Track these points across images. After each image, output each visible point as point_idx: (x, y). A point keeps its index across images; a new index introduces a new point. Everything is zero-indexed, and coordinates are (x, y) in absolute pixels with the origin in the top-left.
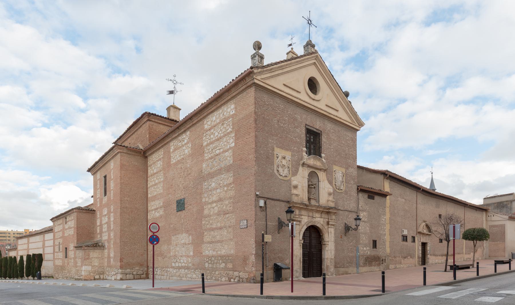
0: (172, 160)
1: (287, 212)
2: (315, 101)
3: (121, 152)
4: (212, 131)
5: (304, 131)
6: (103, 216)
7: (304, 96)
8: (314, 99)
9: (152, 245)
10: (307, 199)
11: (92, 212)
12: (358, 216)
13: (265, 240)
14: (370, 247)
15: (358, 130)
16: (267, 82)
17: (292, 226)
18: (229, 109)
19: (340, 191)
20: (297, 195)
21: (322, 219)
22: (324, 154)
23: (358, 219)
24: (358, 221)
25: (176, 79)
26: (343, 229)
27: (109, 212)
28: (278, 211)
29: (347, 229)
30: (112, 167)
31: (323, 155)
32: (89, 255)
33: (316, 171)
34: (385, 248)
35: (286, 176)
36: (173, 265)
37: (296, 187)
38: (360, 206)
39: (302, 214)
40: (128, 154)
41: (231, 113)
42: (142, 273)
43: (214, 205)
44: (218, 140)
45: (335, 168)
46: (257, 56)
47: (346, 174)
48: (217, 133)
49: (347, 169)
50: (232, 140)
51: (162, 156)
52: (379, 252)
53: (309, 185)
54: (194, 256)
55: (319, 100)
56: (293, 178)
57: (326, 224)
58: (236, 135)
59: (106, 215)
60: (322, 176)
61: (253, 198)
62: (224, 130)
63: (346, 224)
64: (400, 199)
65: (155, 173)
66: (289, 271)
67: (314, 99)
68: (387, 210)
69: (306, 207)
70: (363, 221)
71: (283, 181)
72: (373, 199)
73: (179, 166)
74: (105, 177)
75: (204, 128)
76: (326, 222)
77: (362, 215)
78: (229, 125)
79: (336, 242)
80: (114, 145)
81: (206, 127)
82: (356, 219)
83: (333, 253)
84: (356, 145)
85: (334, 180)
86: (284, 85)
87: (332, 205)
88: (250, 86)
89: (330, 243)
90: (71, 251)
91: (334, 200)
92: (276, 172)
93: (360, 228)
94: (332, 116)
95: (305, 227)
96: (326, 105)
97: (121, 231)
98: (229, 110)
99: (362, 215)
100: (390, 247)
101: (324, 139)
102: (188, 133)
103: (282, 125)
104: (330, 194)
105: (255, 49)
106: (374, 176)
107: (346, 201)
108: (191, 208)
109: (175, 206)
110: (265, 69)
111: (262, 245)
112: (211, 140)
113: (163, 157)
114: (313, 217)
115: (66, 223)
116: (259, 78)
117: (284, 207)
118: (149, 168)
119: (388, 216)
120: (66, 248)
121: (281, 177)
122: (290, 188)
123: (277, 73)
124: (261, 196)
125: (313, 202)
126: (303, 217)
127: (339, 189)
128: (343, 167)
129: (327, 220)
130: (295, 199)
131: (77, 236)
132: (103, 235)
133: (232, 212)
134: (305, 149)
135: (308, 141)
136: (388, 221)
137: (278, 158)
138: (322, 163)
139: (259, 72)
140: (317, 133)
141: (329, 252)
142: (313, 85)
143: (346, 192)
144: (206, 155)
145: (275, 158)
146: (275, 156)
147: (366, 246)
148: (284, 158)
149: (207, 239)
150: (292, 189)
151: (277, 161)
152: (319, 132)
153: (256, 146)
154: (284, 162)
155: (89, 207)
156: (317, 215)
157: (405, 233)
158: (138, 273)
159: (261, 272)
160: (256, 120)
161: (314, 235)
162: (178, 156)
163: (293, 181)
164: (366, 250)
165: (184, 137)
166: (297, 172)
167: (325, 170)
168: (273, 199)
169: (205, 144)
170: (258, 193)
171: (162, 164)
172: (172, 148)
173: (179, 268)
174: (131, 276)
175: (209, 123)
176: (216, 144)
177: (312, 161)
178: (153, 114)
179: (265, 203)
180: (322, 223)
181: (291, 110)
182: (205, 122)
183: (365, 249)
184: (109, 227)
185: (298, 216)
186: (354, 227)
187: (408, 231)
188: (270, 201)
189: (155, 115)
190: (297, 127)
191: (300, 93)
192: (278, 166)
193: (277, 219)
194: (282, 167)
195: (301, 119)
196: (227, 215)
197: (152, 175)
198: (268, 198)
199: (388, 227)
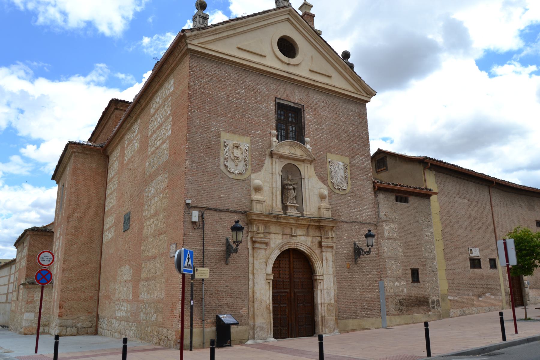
2: (290, 66)
3: (75, 152)
5: (272, 107)
7: (273, 61)
8: (288, 64)
10: (280, 205)
11: (49, 234)
14: (407, 281)
15: (368, 102)
16: (208, 46)
18: (170, 86)
20: (260, 202)
21: (310, 239)
24: (370, 239)
26: (351, 253)
28: (220, 229)
29: (358, 252)
31: (307, 139)
32: (33, 297)
33: (296, 163)
35: (241, 174)
37: (258, 189)
38: (381, 214)
39: (271, 231)
40: (84, 153)
42: (90, 325)
45: (330, 157)
46: (198, 17)
47: (352, 166)
52: (425, 288)
55: (297, 65)
56: (253, 176)
57: (317, 246)
60: (308, 172)
61: (182, 208)
62: (164, 113)
63: (355, 244)
64: (458, 199)
67: (288, 64)
68: (436, 218)
69: (272, 220)
72: (407, 202)
76: (317, 243)
77: (387, 228)
79: (338, 275)
83: (332, 294)
84: (366, 122)
87: (326, 214)
88: (185, 55)
89: (325, 278)
91: (330, 207)
92: (222, 167)
95: (277, 253)
96: (310, 70)
97: (64, 261)
101: (308, 117)
102: (139, 121)
104: (322, 197)
106: (409, 167)
108: (134, 226)
110: (204, 31)
111: (190, 288)
114: (291, 236)
116: (195, 42)
119: (437, 227)
123: (225, 34)
124: (195, 205)
125: (291, 212)
126: (272, 236)
127: (339, 189)
128: (345, 155)
129: (319, 239)
130: (257, 208)
131: (27, 268)
134: (275, 132)
135: (279, 122)
137: (226, 147)
138: (306, 150)
139: (195, 35)
140: (295, 108)
141: (326, 292)
142: (287, 47)
143: (353, 194)
145: (222, 147)
146: (222, 144)
147: (398, 279)
148: (237, 147)
150: (253, 192)
151: (225, 152)
152: (300, 107)
153: (189, 132)
154: (237, 153)
155: (48, 228)
156: (300, 232)
157: (476, 253)
158: (84, 326)
160: (189, 97)
163: (254, 180)
164: (398, 286)
166: (262, 166)
167: (311, 162)
168: (216, 210)
170: (189, 201)
174: (74, 330)
177: (287, 149)
179: (202, 216)
180: (309, 244)
181: (249, 80)
183: (397, 284)
186: (366, 249)
190: (261, 102)
191: (265, 57)
192: (226, 159)
193: (224, 241)
194: (233, 161)
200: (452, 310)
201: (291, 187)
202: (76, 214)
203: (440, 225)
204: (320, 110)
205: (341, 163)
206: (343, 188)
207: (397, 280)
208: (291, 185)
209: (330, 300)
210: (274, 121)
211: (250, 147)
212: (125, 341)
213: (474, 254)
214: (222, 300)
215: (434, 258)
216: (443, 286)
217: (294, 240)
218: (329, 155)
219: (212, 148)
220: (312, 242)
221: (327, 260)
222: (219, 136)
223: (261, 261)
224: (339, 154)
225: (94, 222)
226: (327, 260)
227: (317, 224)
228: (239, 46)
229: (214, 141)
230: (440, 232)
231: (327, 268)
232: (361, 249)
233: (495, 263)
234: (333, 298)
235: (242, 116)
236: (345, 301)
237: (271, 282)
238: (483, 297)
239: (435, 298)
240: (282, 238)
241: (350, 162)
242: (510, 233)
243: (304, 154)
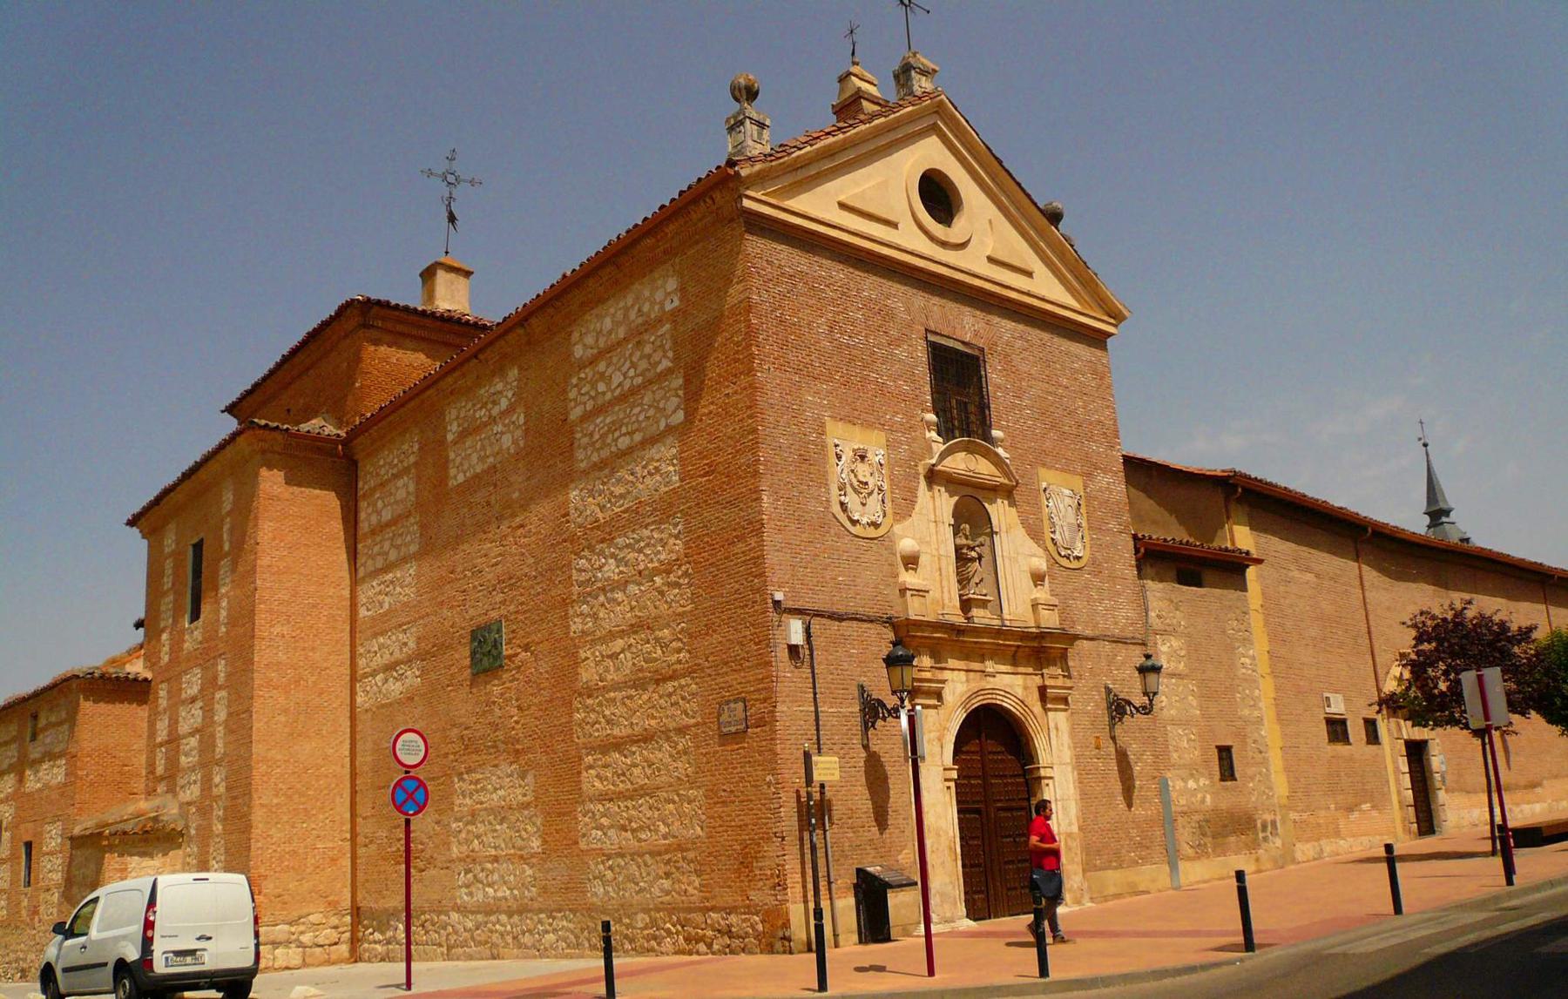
0: (453, 472)
1: (891, 661)
4: (602, 366)
5: (922, 354)
6: (183, 702)
7: (911, 237)
9: (403, 818)
12: (1148, 657)
13: (818, 777)
14: (1211, 776)
16: (791, 204)
17: (911, 720)
19: (1075, 564)
20: (921, 592)
21: (1019, 680)
22: (1000, 428)
23: (1148, 670)
24: (1152, 677)
25: (455, 166)
27: (210, 684)
29: (1118, 708)
30: (227, 507)
31: (996, 433)
34: (1268, 776)
36: (463, 896)
37: (911, 562)
38: (1152, 614)
41: (668, 307)
43: (619, 644)
44: (623, 398)
47: (1089, 498)
48: (619, 377)
49: (1088, 476)
50: (675, 400)
51: (412, 459)
53: (958, 549)
54: (545, 854)
56: (897, 528)
57: (1036, 695)
58: (687, 381)
59: (193, 700)
60: (1000, 512)
62: (643, 365)
63: (1108, 691)
64: (1296, 574)
65: (388, 525)
66: (914, 895)
68: (1256, 621)
70: (1172, 675)
71: (862, 542)
73: (479, 497)
74: (198, 548)
75: (570, 354)
77: (1164, 649)
78: (662, 346)
80: (232, 424)
81: (578, 351)
82: (1142, 670)
85: (1046, 523)
87: (1050, 620)
90: (51, 853)
93: (1162, 700)
94: (1014, 295)
95: (960, 716)
98: (659, 295)
99: (1166, 651)
100: (1287, 769)
101: (994, 375)
103: (845, 339)
104: (1038, 578)
105: (737, 100)
107: (1101, 601)
109: (463, 654)
112: (600, 402)
113: (416, 463)
115: (34, 738)
117: (881, 641)
118: (363, 504)
120: (29, 845)
121: (856, 530)
124: (790, 604)
128: (1074, 472)
130: (915, 609)
132: (181, 782)
133: (689, 672)
134: (932, 417)
136: (1264, 666)
137: (839, 457)
138: (997, 461)
140: (967, 355)
142: (937, 196)
143: (1096, 567)
144: (580, 454)
146: (832, 451)
147: (1192, 771)
149: (592, 782)
151: (839, 471)
152: (976, 353)
154: (863, 471)
157: (1338, 707)
158: (321, 941)
161: (994, 740)
162: (474, 457)
165: (500, 386)
166: (913, 503)
169: (576, 413)
171: (412, 488)
172: (454, 427)
173: (489, 910)
175: (589, 340)
176: (618, 412)
177: (960, 463)
178: (379, 302)
181: (870, 286)
182: (576, 335)
183: (1191, 784)
184: (207, 745)
185: (928, 675)
187: (1347, 700)
188: (824, 621)
189: (387, 305)
190: (895, 343)
195: (908, 311)
196: (670, 686)
197: (373, 532)
198: (819, 614)
199: (1266, 690)
200: (1299, 845)
201: (974, 554)
202: (277, 630)
203: (1265, 639)
204: (1016, 359)
205: (1067, 492)
207: (1192, 775)
208: (973, 549)
210: (928, 388)
213: (1333, 710)
215: (1260, 721)
216: (1281, 786)
217: (991, 683)
218: (1042, 472)
220: (1026, 688)
224: (1062, 470)
225: (326, 649)
227: (1035, 644)
230: (1266, 656)
232: (879, 701)
233: (1376, 731)
234: (1074, 820)
235: (864, 379)
237: (952, 784)
238: (1356, 814)
239: (1268, 817)
242: (1403, 656)
243: (997, 473)
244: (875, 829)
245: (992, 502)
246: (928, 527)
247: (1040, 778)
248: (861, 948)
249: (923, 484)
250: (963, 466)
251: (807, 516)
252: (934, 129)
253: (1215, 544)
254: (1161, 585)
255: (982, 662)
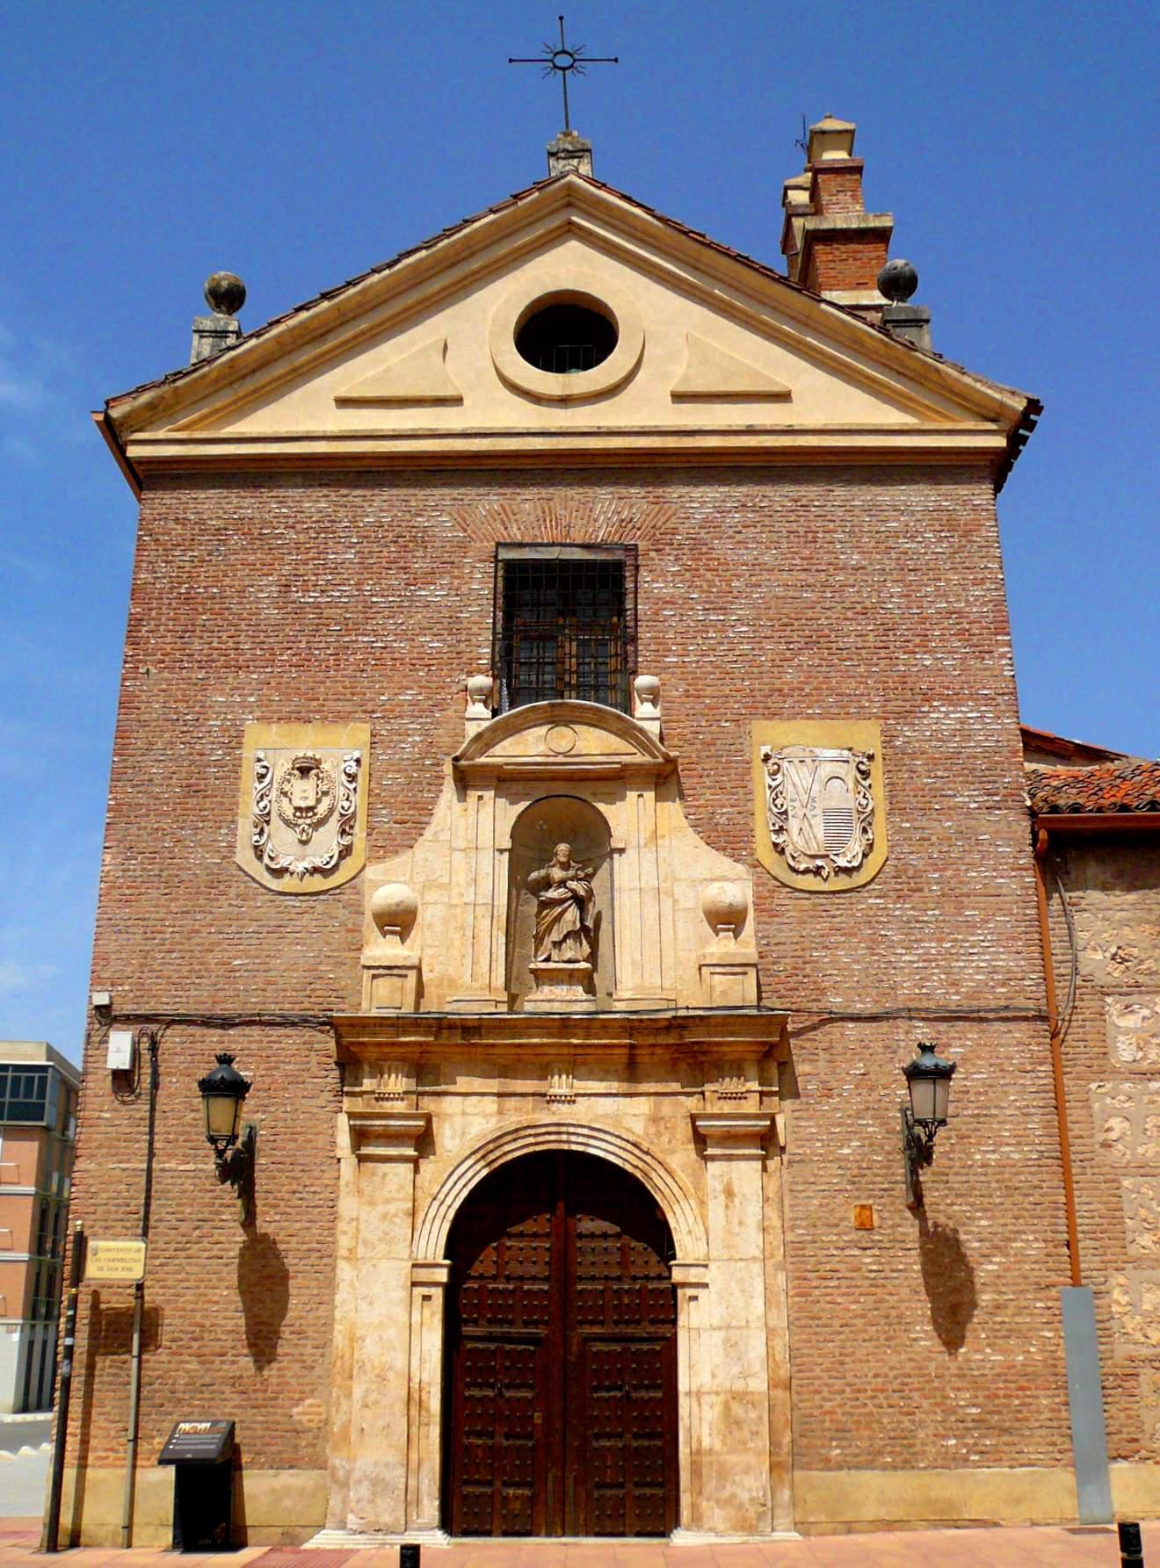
21: (642, 1105)
37: (399, 921)
45: (767, 735)
47: (896, 756)
77: (1130, 1021)
86: (678, 397)
104: (727, 919)
122: (356, 930)
127: (817, 871)
128: (862, 715)
140: (604, 565)
141: (725, 1344)
142: (566, 334)
146: (249, 770)
152: (619, 555)
154: (304, 792)
159: (925, 1176)
163: (378, 885)
166: (420, 827)
168: (187, 1021)
181: (379, 506)
190: (430, 577)
204: (722, 548)
206: (842, 862)
209: (744, 1376)
211: (365, 762)
212: (1076, 1281)
214: (216, 1366)
219: (206, 791)
221: (729, 1193)
222: (235, 740)
223: (392, 1208)
226: (729, 1193)
228: (344, 392)
229: (218, 764)
231: (729, 1232)
236: (838, 1384)
237: (438, 1294)
240: (500, 1112)
241: (888, 742)
244: (247, 1362)
245: (612, 798)
246: (460, 861)
247: (675, 1287)
248: (178, 1557)
249: (449, 787)
250: (542, 748)
251: (184, 875)
252: (570, 231)
253: (601, 807)
254: (1133, 897)
255: (543, 1077)
